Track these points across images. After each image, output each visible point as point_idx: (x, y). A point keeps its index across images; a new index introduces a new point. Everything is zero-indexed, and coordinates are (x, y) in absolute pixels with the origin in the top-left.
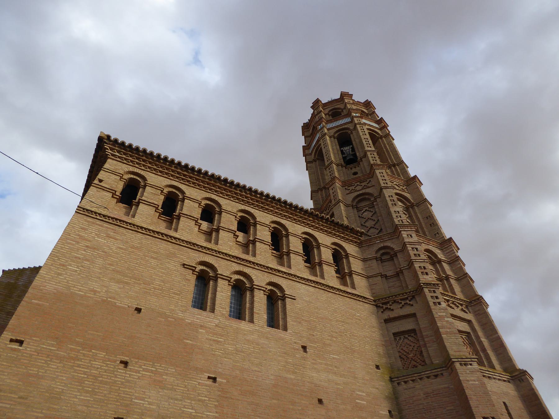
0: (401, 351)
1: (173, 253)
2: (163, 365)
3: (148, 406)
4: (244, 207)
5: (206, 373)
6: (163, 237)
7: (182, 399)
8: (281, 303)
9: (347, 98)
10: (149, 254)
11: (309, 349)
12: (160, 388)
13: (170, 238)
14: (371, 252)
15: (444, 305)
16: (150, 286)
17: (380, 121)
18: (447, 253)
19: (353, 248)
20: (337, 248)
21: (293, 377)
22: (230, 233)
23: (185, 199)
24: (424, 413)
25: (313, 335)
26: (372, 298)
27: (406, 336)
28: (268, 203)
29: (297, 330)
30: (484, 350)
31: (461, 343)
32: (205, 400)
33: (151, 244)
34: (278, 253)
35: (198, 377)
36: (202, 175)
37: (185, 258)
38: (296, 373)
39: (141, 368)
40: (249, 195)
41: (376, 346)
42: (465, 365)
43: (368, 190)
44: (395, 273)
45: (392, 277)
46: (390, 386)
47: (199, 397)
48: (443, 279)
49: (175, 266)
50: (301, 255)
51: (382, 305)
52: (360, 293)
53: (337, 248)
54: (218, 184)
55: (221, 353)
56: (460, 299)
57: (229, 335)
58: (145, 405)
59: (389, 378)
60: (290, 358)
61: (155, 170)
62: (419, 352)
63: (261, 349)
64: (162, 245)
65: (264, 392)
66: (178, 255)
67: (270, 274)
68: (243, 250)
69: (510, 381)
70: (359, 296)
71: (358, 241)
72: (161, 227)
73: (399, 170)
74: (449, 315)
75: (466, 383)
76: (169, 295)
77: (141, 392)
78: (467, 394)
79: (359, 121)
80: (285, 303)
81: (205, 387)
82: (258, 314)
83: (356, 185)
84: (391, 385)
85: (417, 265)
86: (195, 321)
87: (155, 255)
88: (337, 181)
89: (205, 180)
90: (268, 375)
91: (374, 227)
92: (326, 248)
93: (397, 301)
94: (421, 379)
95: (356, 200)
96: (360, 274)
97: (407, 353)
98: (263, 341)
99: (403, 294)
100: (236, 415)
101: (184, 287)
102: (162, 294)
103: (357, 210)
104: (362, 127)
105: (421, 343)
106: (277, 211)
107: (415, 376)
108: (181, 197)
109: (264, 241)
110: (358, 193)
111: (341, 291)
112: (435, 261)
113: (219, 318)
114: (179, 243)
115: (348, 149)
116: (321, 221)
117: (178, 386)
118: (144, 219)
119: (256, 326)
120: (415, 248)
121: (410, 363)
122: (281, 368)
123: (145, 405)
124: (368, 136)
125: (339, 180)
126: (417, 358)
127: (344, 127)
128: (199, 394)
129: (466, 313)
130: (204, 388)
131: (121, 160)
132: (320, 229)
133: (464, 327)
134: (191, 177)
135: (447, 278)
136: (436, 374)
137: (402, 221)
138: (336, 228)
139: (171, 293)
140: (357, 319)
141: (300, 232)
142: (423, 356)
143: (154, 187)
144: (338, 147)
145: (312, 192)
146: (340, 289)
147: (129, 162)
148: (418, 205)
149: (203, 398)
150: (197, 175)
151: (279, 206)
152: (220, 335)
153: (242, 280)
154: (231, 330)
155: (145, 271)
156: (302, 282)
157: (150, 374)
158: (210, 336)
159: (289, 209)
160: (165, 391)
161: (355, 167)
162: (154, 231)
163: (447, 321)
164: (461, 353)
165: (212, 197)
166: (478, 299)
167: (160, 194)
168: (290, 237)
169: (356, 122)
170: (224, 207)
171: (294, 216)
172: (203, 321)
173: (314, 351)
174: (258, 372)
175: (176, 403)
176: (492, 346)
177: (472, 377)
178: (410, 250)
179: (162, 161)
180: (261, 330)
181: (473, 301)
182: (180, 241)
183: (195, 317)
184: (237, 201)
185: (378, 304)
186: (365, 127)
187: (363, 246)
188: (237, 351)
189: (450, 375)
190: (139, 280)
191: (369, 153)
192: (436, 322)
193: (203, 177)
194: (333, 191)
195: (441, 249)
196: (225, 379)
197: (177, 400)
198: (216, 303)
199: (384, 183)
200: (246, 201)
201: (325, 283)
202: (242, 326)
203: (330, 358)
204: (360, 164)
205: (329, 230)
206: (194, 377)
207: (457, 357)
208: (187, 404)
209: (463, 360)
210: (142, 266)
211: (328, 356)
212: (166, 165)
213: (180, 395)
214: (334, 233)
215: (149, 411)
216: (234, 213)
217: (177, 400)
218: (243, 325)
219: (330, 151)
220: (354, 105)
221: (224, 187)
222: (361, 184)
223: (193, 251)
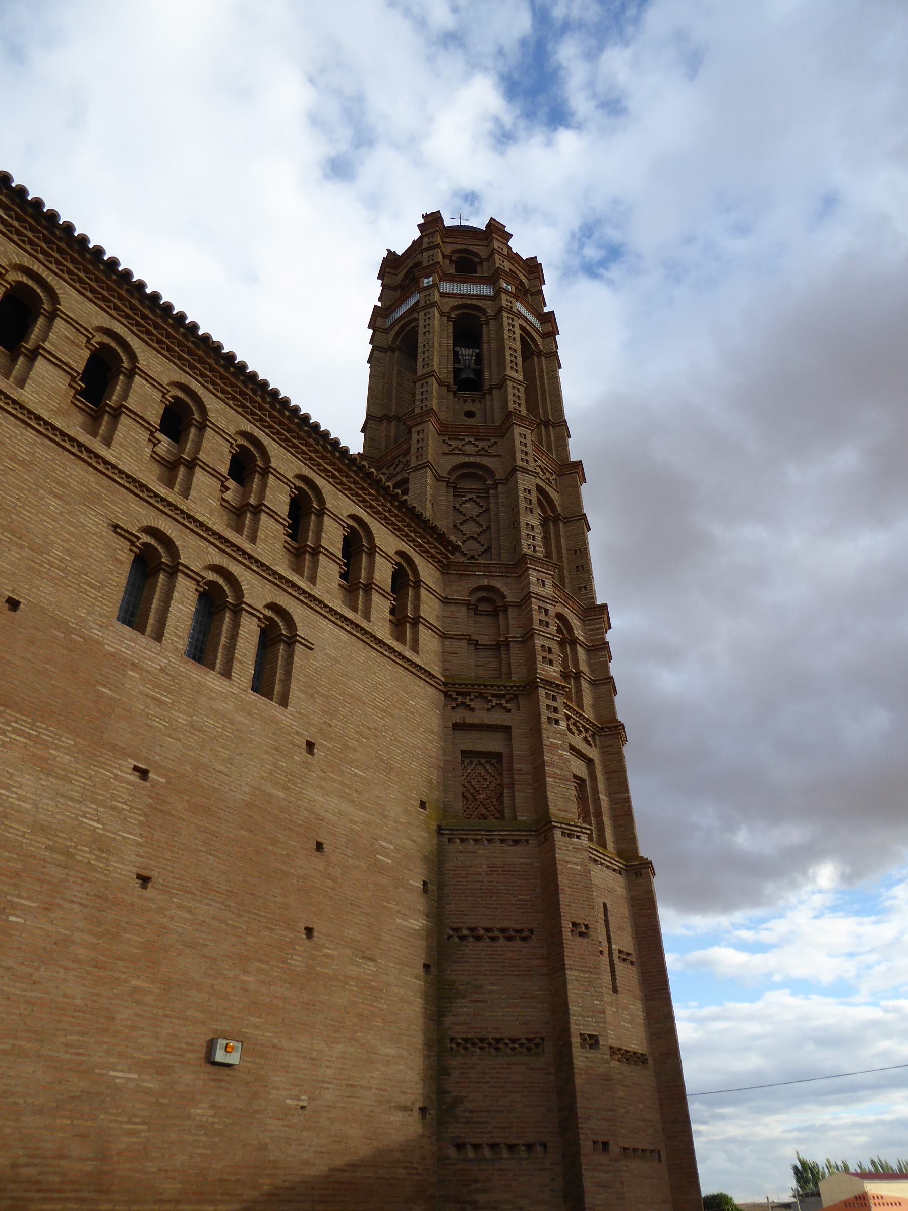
0: (467, 785)
1: (96, 494)
2: (53, 729)
3: (17, 803)
4: (251, 428)
5: (132, 758)
6: (81, 451)
7: (81, 800)
8: (283, 650)
9: (499, 238)
10: (48, 483)
11: (318, 749)
12: (42, 771)
13: (95, 457)
14: (461, 590)
15: (563, 725)
16: (42, 556)
17: (549, 319)
18: (590, 630)
19: (432, 572)
20: (403, 563)
21: (282, 795)
22: (215, 479)
23: (136, 373)
24: (481, 897)
25: (330, 725)
26: (443, 679)
27: (483, 761)
28: (301, 434)
29: (304, 710)
30: (599, 814)
31: (572, 798)
32: (123, 809)
33: (53, 460)
34: (294, 544)
35: (115, 763)
36: (182, 330)
37: (119, 512)
38: (288, 789)
39: (10, 725)
40: (267, 406)
41: (429, 767)
42: (570, 836)
43: (486, 461)
44: (494, 643)
45: (486, 647)
46: (435, 841)
47: (113, 803)
48: (571, 675)
49: (97, 524)
50: (338, 561)
52: (425, 663)
53: (403, 563)
54: (211, 361)
55: (162, 724)
56: (588, 720)
57: (184, 693)
58: (10, 800)
59: (436, 828)
60: (283, 760)
61: (81, 281)
62: (496, 793)
63: (236, 733)
64: (75, 470)
65: (229, 813)
66: (107, 500)
67: (276, 588)
68: (229, 519)
69: (623, 871)
70: (421, 668)
71: (445, 561)
72: (73, 425)
73: (552, 438)
74: (567, 747)
75: (563, 865)
76: (79, 585)
77: (6, 774)
78: (559, 883)
79: (509, 304)
80: (293, 651)
81: (125, 785)
82: (241, 662)
83: (466, 440)
84: (436, 839)
85: (539, 642)
86: (123, 652)
87: (59, 490)
88: (433, 420)
89: (186, 343)
90: (241, 783)
91: (476, 539)
92: (384, 560)
93: (485, 695)
94: (489, 841)
95: (458, 473)
96: (432, 627)
97: (476, 791)
98: (242, 719)
99: (499, 686)
100: (174, 847)
101: (110, 576)
102: (64, 581)
103: (454, 492)
104: (512, 320)
105: (505, 780)
106: (313, 455)
107: (481, 835)
108: (125, 365)
109: (276, 513)
110: (467, 459)
111: (395, 651)
112: (567, 640)
113: (170, 655)
114: (111, 475)
115: (469, 355)
116: (383, 496)
117: (76, 774)
118: (43, 398)
119: (234, 685)
120: (545, 609)
121: (476, 809)
122: (266, 775)
123: (10, 800)
124: (517, 345)
125: (438, 420)
126: (490, 804)
127: (475, 302)
128: (113, 798)
129: (590, 745)
130: (123, 788)
131: (6, 231)
132: (383, 516)
133: (579, 768)
134: (157, 326)
135: (578, 676)
136: (517, 838)
137: (534, 547)
138: (413, 525)
139: (83, 583)
140: (408, 710)
141: (345, 514)
142: (502, 803)
143: (74, 324)
144: (452, 342)
145: (369, 417)
146: (393, 649)
147: (164, 349)
148: (567, 521)
149: (120, 805)
150: (172, 326)
151: (319, 448)
152: (167, 690)
153: (221, 585)
154: (187, 685)
155: (36, 521)
156: (330, 617)
157: (25, 741)
158: (148, 688)
159: (338, 458)
160: (51, 779)
161: (473, 401)
162: (63, 434)
163: (561, 756)
164: (568, 815)
165: (191, 386)
166: (616, 727)
167: (83, 345)
168: (326, 518)
169: (504, 303)
170: (212, 416)
171: (342, 476)
172: (137, 654)
173: (327, 754)
174: (225, 774)
175: (70, 806)
176: (612, 809)
177: (574, 857)
178: (535, 610)
179: (102, 267)
180: (242, 696)
181: (607, 727)
182: (114, 471)
183: (122, 642)
184: (240, 410)
185: (450, 691)
186: (518, 322)
187: (450, 572)
188: (192, 727)
189: (539, 845)
190: (20, 538)
191: (510, 384)
192: (542, 752)
193: (184, 335)
194: (420, 437)
195: (582, 621)
196: (164, 776)
197: (71, 799)
198: (168, 623)
199: (522, 459)
200: (259, 415)
201: (370, 630)
202: (210, 682)
203: (350, 773)
204: (484, 397)
205: (399, 524)
206: (107, 762)
207: (561, 820)
208: (90, 811)
209: (569, 827)
210: (30, 507)
211: (347, 768)
212: (109, 278)
213: (78, 792)
214: (406, 533)
215: (17, 811)
216: (230, 436)
217: (71, 799)
218: (210, 679)
219: (433, 347)
220: (509, 261)
221: (222, 370)
222: (477, 443)
223: (137, 500)
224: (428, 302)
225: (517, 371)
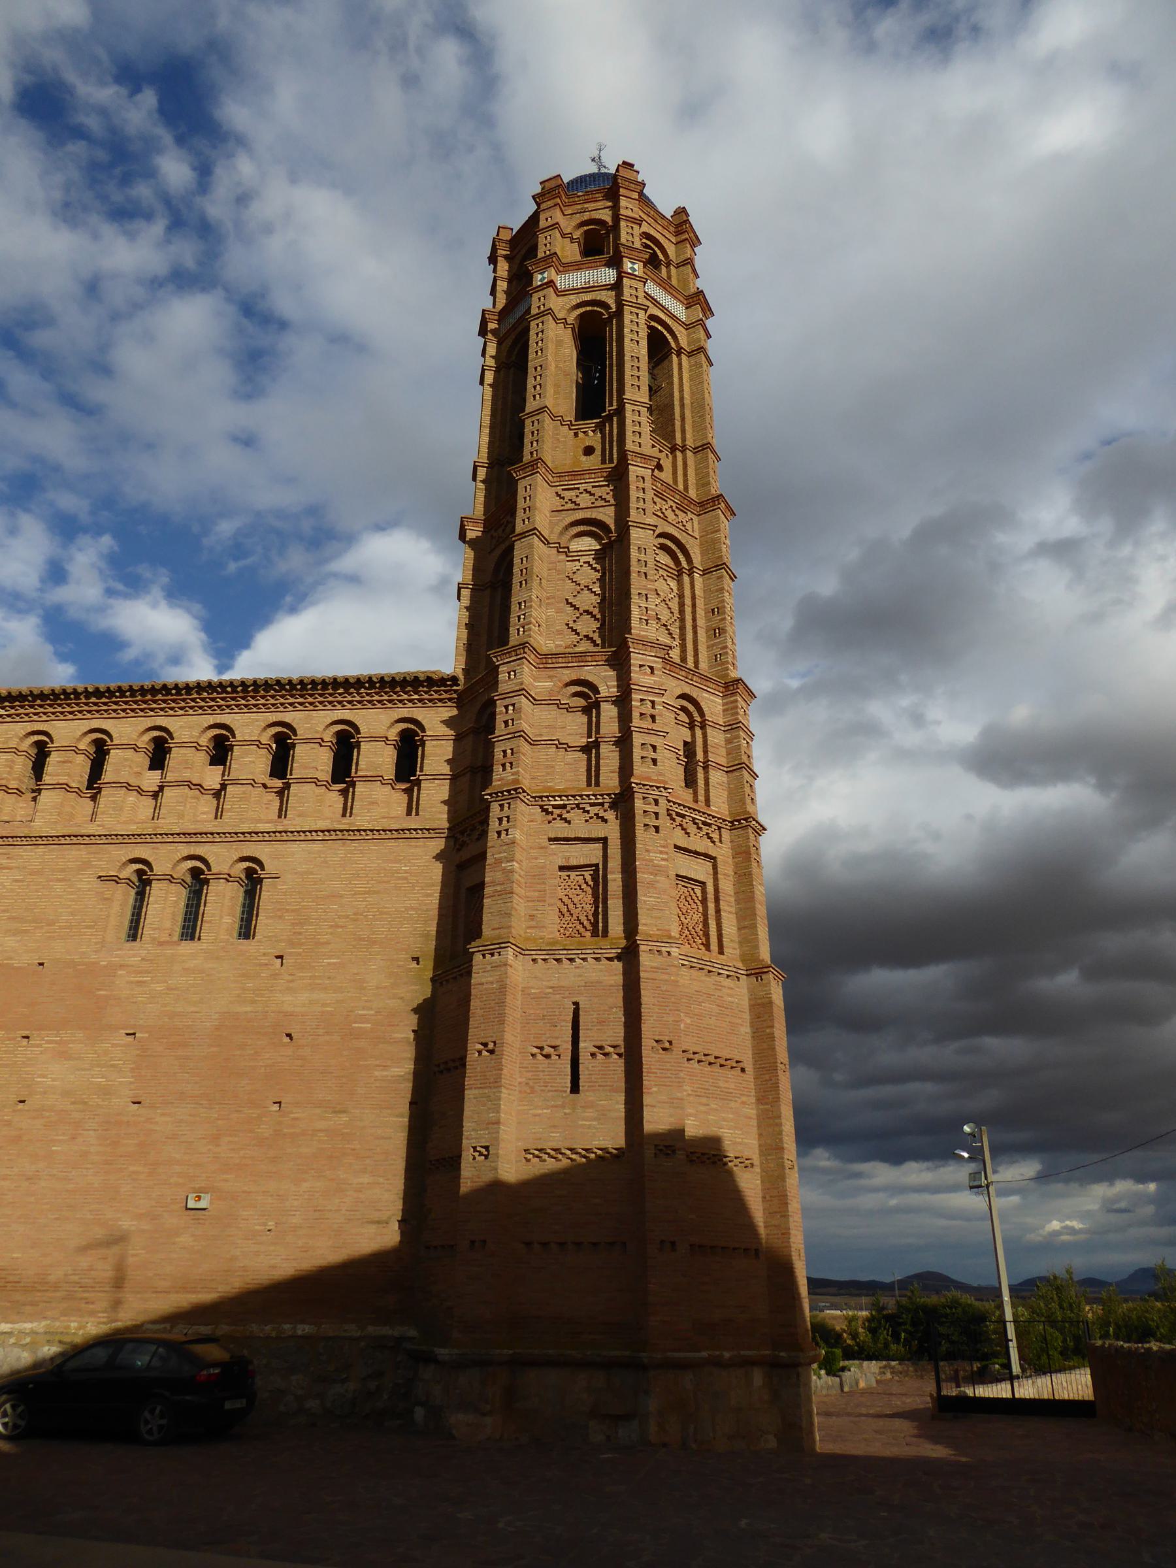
5: (122, 1029)
51: (703, 824)
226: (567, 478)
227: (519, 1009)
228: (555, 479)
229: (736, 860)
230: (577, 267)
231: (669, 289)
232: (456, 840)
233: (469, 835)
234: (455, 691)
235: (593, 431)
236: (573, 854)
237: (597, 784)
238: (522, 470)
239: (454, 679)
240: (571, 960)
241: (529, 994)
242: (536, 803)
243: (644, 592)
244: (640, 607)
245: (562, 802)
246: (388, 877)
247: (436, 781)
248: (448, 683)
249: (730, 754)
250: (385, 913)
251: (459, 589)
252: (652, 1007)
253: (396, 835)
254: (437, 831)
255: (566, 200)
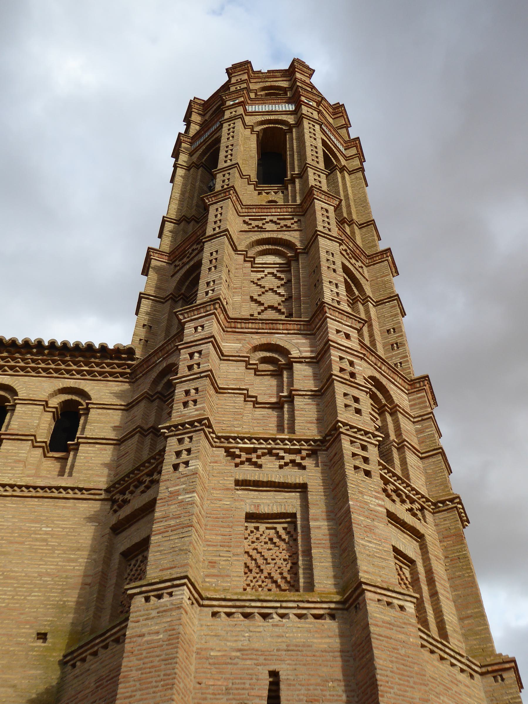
103: (252, 267)
104: (319, 176)
187: (137, 377)
224: (217, 230)
225: (358, 411)
226: (254, 210)
227: (192, 678)
228: (244, 210)
229: (445, 544)
230: (262, 102)
231: (333, 132)
232: (113, 501)
233: (132, 493)
234: (129, 366)
235: (276, 193)
236: (264, 501)
237: (292, 430)
238: (214, 196)
239: (130, 351)
240: (265, 616)
241: (207, 659)
242: (222, 445)
243: (334, 282)
244: (332, 291)
245: (252, 446)
246: (23, 537)
247: (97, 446)
248: (123, 356)
249: (423, 442)
250: (13, 578)
251: (140, 298)
252: (390, 674)
253: (41, 493)
254: (92, 492)
255: (253, 75)
